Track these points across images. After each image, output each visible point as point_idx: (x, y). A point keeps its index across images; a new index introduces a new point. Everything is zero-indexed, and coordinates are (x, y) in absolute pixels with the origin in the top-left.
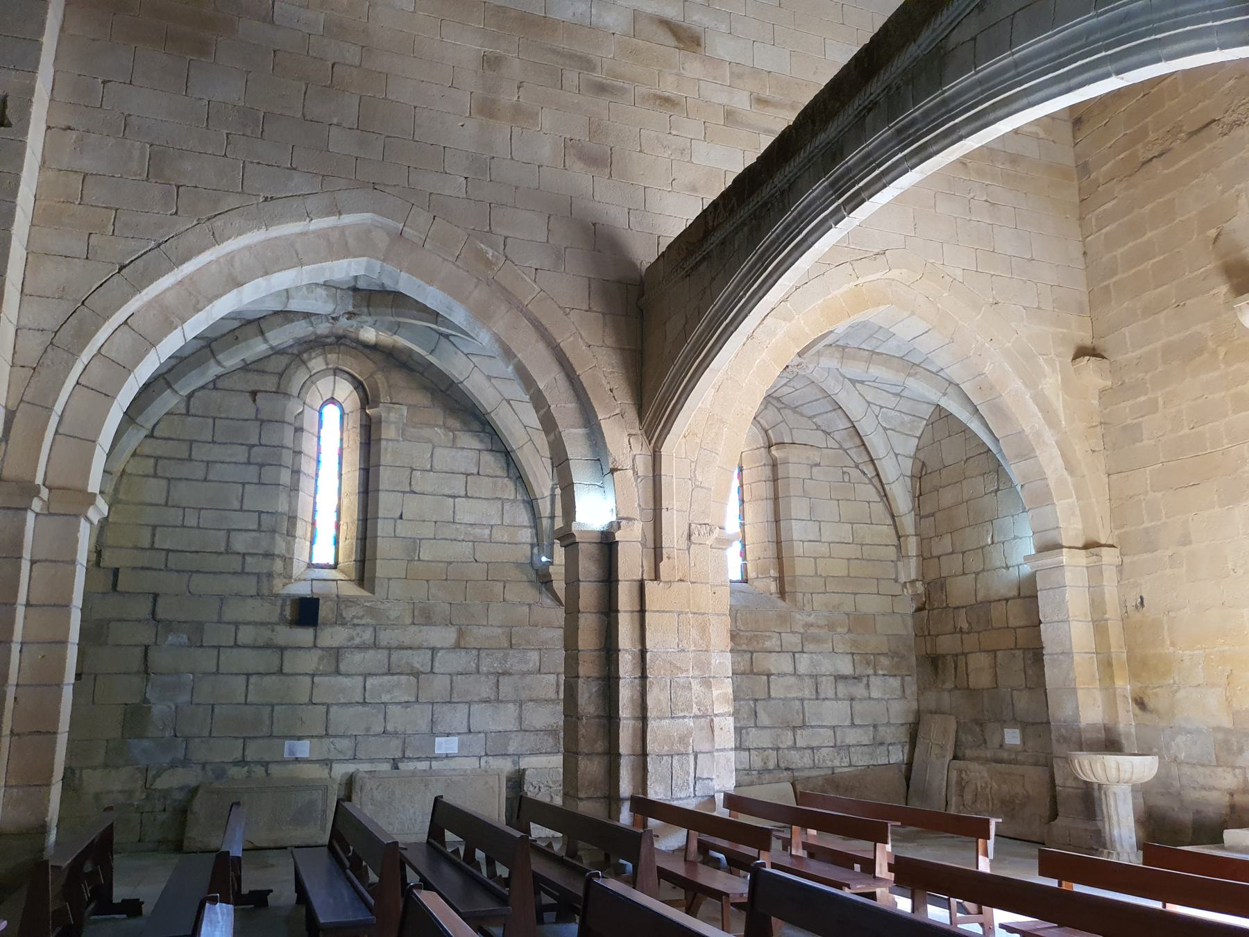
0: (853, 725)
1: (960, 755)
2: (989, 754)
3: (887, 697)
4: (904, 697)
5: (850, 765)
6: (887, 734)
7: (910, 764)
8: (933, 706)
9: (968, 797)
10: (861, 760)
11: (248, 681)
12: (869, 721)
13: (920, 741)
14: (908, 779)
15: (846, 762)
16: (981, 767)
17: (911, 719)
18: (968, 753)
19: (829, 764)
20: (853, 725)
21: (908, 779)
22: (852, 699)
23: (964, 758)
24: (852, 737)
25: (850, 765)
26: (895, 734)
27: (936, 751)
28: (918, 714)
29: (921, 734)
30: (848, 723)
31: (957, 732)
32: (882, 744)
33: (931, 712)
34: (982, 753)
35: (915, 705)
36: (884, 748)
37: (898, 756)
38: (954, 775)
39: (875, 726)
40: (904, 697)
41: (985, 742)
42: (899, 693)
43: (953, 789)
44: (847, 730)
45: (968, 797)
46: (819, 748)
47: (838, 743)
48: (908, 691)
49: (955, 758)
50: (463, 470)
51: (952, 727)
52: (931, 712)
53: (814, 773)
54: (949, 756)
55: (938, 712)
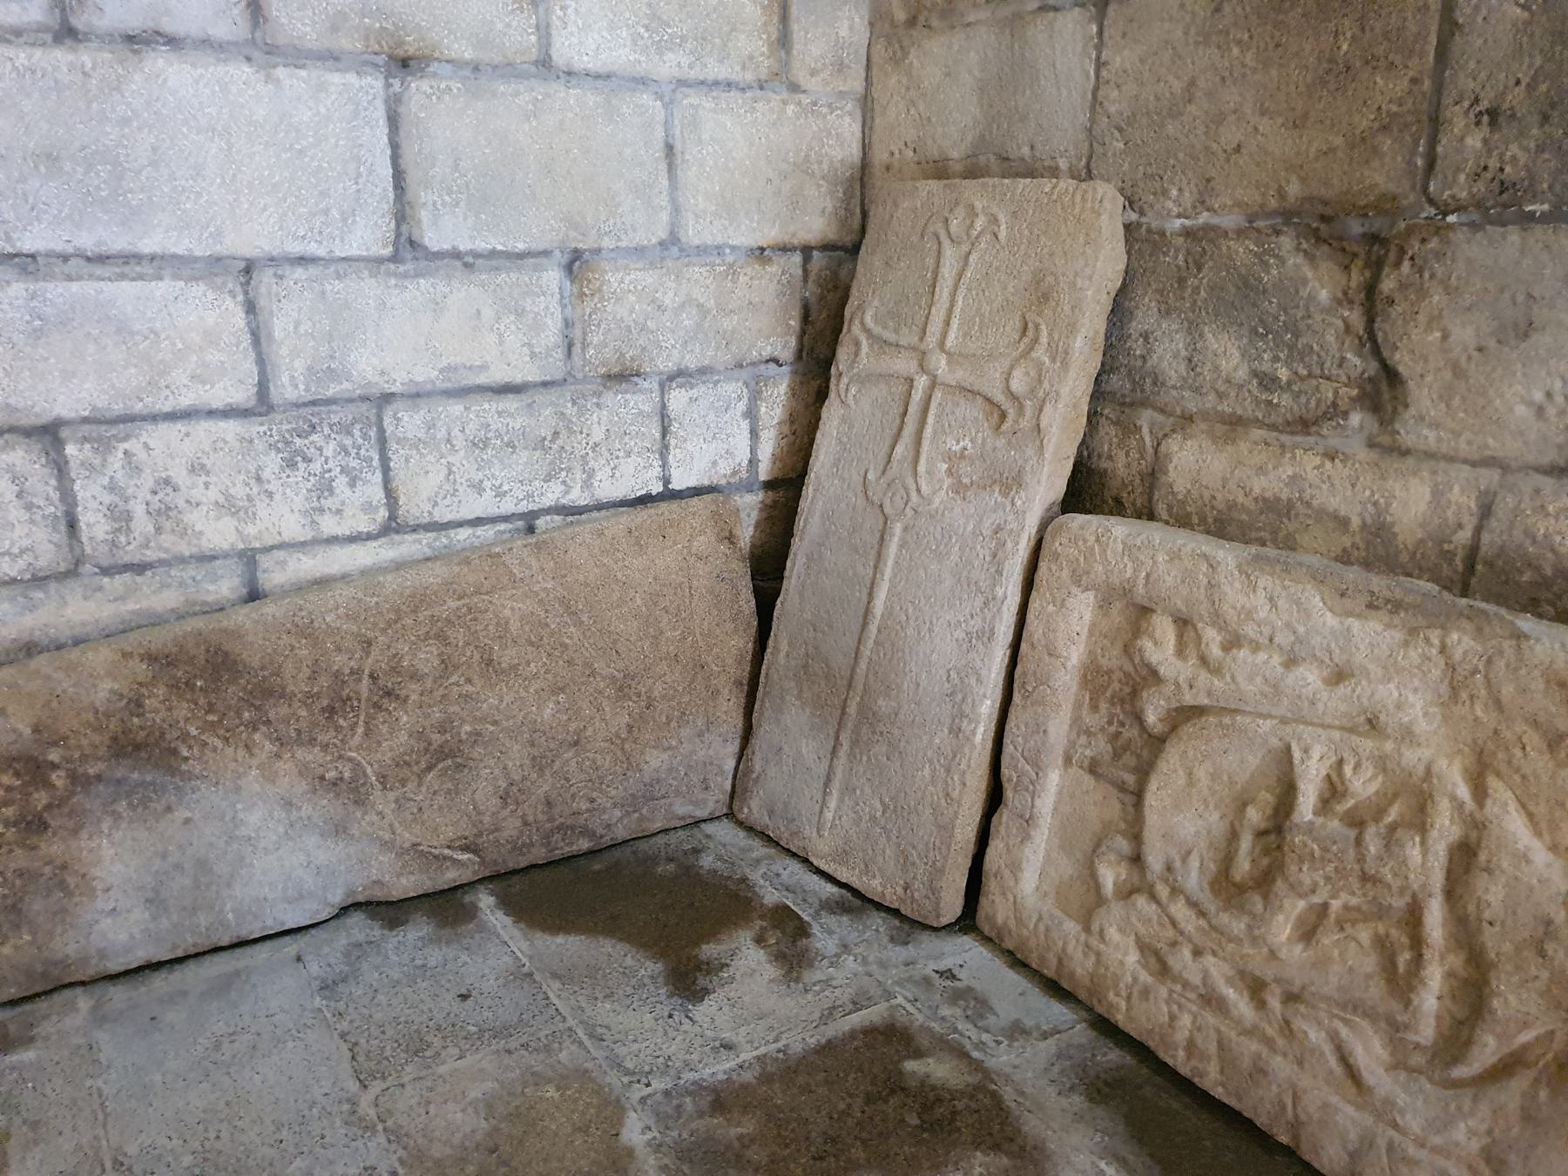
0: (407, 249)
1: (1121, 464)
2: (1411, 503)
3: (671, 64)
4: (781, 77)
5: (393, 526)
6: (653, 308)
7: (787, 487)
8: (954, 136)
9: (1186, 813)
10: (466, 479)
11: (402, 212)
12: (535, 228)
13: (856, 358)
14: (768, 568)
15: (358, 504)
16: (1371, 636)
17: (815, 224)
18: (1193, 463)
19: (219, 533)
20: (407, 249)
21: (768, 568)
22: (404, 64)
23: (1142, 501)
24: (400, 335)
25: (393, 526)
26: (716, 323)
27: (956, 433)
28: (861, 190)
29: (867, 314)
30: (369, 234)
31: (1119, 311)
32: (622, 377)
33: (939, 170)
34: (1334, 480)
35: (842, 139)
36: (638, 402)
37: (724, 441)
38: (1073, 627)
39: (576, 264)
40: (781, 77)
41: (1384, 390)
42: (752, 45)
43: (1058, 719)
44: (367, 289)
45: (1186, 813)
46: (109, 426)
47: (289, 385)
48: (811, 46)
49: (1086, 491)
50: (569, 97)
51: (1107, 264)
52: (939, 170)
53: (78, 609)
54: (1050, 482)
55: (992, 162)
